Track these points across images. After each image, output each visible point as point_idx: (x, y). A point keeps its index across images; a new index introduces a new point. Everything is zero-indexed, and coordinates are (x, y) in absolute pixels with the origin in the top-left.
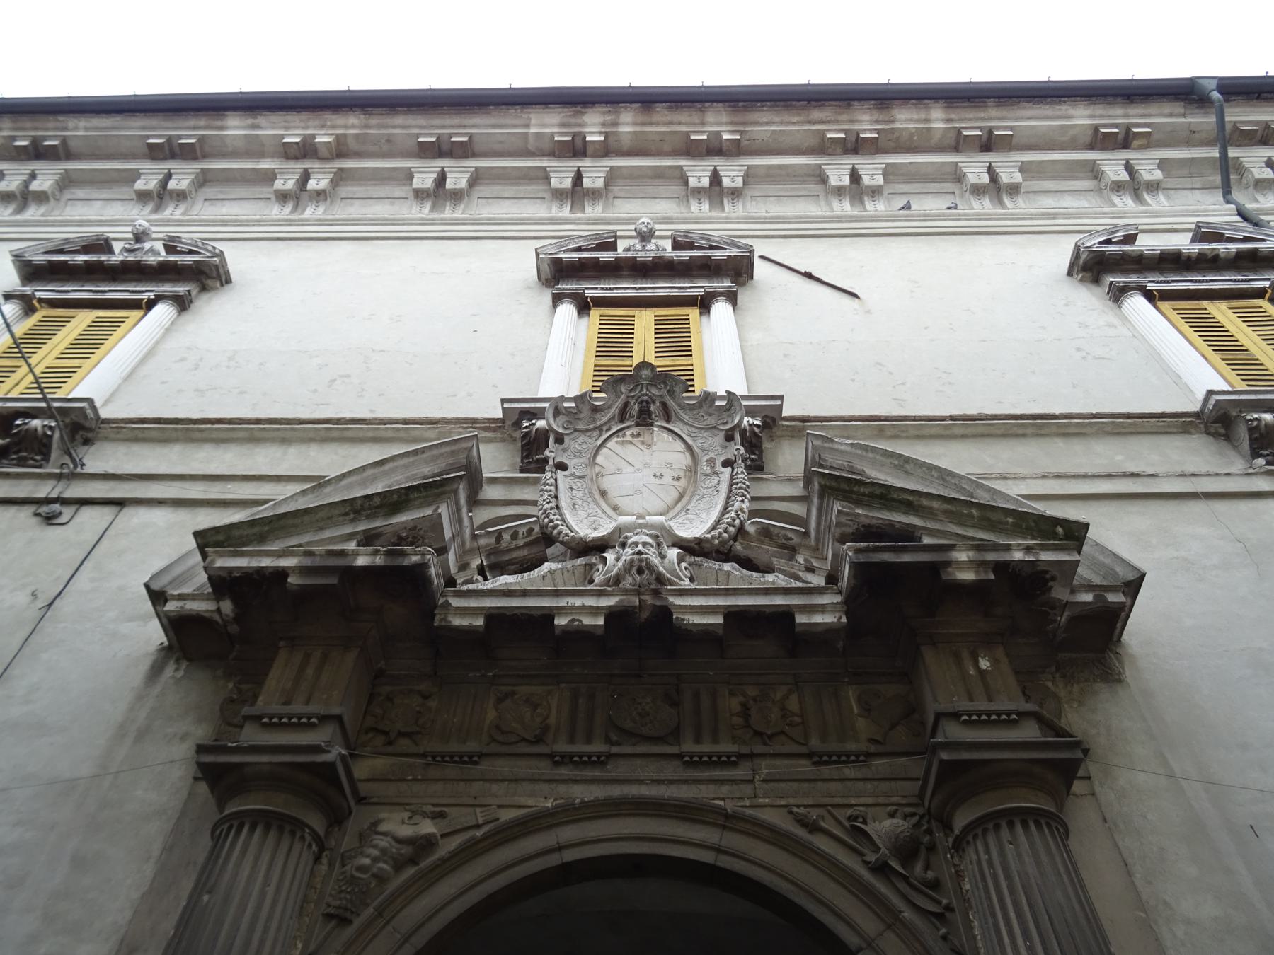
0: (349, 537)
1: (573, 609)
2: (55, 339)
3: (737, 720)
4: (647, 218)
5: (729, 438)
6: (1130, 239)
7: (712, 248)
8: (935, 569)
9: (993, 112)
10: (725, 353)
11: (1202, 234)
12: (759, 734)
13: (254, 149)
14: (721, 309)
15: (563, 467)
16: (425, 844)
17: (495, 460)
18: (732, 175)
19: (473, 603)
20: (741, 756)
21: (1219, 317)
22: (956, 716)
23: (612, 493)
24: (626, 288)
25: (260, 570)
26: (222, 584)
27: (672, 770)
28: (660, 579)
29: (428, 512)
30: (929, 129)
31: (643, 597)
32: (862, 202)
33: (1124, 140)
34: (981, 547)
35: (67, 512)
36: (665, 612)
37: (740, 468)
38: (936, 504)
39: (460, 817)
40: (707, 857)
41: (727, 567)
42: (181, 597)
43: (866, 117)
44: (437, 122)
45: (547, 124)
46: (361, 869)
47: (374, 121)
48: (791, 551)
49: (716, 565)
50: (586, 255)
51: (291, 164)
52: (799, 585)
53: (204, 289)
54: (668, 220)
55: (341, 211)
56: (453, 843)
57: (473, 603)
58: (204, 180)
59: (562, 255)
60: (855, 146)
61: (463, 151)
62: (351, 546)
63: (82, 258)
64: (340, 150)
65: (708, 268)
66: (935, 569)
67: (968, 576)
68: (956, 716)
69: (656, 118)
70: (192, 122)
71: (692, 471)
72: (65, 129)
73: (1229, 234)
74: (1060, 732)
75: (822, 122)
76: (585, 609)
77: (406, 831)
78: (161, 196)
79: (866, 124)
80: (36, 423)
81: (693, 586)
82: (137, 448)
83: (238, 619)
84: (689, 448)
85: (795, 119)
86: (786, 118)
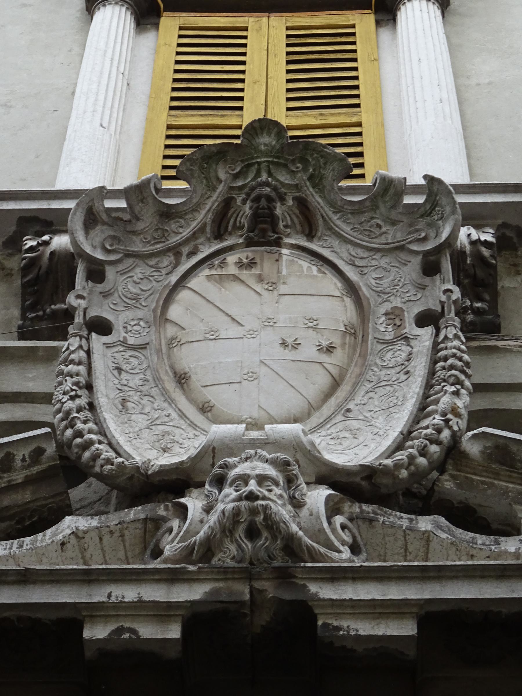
1: (120, 609)
5: (430, 268)
15: (102, 327)
23: (197, 380)
28: (291, 547)
31: (258, 585)
36: (302, 614)
37: (452, 330)
41: (425, 523)
49: (404, 520)
71: (357, 334)
81: (358, 562)
84: (352, 289)
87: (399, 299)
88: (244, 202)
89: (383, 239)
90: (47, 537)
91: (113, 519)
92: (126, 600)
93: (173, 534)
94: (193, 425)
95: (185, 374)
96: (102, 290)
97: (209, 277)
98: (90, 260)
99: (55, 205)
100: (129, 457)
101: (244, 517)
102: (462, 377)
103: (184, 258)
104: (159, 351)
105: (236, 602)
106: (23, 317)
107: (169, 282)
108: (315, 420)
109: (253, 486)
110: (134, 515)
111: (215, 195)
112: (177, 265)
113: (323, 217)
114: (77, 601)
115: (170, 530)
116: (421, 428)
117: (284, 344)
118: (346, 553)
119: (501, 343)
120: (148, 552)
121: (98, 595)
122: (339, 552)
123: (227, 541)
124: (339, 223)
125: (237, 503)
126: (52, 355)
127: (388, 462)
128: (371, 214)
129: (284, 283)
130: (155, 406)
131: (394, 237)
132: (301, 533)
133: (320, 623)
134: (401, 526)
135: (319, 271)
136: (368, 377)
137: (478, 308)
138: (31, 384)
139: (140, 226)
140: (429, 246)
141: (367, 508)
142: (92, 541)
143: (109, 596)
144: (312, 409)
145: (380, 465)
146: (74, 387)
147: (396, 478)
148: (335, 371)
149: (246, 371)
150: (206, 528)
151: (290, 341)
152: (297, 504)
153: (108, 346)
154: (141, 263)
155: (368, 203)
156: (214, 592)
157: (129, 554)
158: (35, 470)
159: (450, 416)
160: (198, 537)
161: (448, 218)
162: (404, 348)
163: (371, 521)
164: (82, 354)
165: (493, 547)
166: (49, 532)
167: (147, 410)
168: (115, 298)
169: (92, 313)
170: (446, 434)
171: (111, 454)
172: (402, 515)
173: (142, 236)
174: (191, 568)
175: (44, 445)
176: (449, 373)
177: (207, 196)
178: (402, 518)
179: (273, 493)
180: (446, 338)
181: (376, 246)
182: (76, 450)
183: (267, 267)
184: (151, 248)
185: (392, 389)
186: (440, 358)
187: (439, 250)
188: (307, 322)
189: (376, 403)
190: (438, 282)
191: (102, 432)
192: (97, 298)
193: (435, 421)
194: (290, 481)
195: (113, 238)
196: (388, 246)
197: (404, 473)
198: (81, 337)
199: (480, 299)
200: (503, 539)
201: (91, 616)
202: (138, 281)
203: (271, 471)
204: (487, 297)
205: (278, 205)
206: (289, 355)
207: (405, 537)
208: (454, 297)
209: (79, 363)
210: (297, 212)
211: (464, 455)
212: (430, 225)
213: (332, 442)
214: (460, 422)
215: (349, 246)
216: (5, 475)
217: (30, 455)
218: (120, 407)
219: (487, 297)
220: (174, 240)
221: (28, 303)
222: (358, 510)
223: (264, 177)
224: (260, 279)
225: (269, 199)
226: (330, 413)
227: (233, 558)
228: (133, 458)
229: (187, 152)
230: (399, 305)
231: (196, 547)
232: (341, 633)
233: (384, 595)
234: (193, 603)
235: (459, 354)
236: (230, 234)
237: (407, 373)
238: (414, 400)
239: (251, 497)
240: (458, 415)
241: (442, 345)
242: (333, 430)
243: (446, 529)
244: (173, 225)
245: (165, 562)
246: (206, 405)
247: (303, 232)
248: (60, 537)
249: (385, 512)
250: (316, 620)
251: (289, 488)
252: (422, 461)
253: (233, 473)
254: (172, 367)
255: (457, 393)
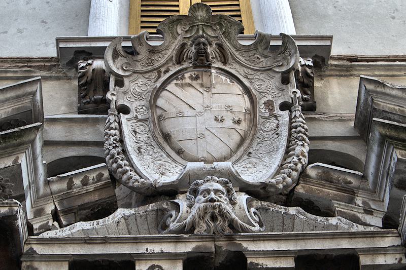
5: (285, 80)
15: (124, 110)
23: (175, 136)
28: (232, 224)
31: (218, 243)
41: (292, 211)
49: (282, 209)
84: (247, 91)
87: (270, 96)
88: (191, 45)
89: (261, 65)
90: (110, 219)
91: (141, 210)
92: (155, 252)
93: (173, 218)
94: (174, 160)
95: (168, 134)
96: (123, 91)
97: (176, 84)
98: (117, 75)
99: (94, 44)
100: (146, 178)
101: (210, 211)
102: (305, 137)
103: (162, 74)
104: (154, 122)
105: (208, 252)
106: (80, 102)
107: (156, 87)
108: (234, 158)
109: (213, 195)
110: (152, 207)
111: (176, 42)
112: (159, 77)
113: (230, 53)
114: (132, 253)
115: (171, 216)
116: (287, 163)
117: (216, 119)
118: (257, 227)
119: (317, 116)
120: (160, 226)
121: (142, 249)
122: (255, 226)
123: (201, 222)
124: (238, 56)
125: (205, 204)
126: (96, 121)
127: (273, 181)
128: (254, 52)
129: (214, 88)
130: (155, 150)
131: (266, 64)
132: (237, 218)
133: (249, 262)
134: (281, 212)
135: (231, 81)
136: (258, 136)
137: (305, 98)
138: (86, 137)
139: (140, 57)
140: (284, 69)
141: (264, 203)
142: (132, 221)
143: (147, 250)
144: (233, 152)
145: (270, 182)
146: (114, 142)
147: (277, 188)
148: (242, 133)
149: (199, 133)
150: (191, 215)
151: (219, 118)
152: (233, 202)
153: (129, 120)
154: (140, 76)
155: (252, 47)
156: (197, 247)
157: (150, 226)
158: (99, 184)
159: (301, 157)
160: (187, 220)
161: (293, 56)
162: (275, 121)
163: (267, 210)
164: (116, 124)
165: (325, 222)
166: (111, 216)
167: (151, 153)
168: (129, 95)
169: (120, 103)
170: (299, 166)
171: (138, 177)
172: (281, 207)
173: (141, 62)
174: (185, 236)
175: (103, 172)
176: (298, 135)
177: (172, 42)
178: (281, 208)
179: (222, 198)
180: (295, 116)
181: (258, 68)
182: (119, 175)
183: (205, 79)
184: (145, 69)
185: (270, 142)
186: (293, 127)
187: (288, 71)
188: (227, 108)
189: (263, 149)
190: (290, 88)
191: (131, 165)
192: (121, 95)
193: (294, 160)
194: (229, 191)
195: (127, 63)
196: (263, 69)
197: (281, 186)
198: (115, 115)
199: (306, 93)
200: (330, 218)
201: (139, 260)
202: (140, 86)
203: (220, 187)
204: (309, 93)
205: (209, 47)
206: (220, 125)
207: (283, 217)
208: (298, 96)
209: (115, 129)
210: (218, 50)
211: (308, 176)
212: (285, 58)
213: (243, 169)
214: (305, 159)
215: (244, 68)
216: (85, 187)
217: (96, 177)
218: (138, 152)
219: (309, 93)
220: (157, 65)
221: (82, 95)
222: (260, 204)
223: (201, 33)
224: (202, 85)
225: (204, 44)
226: (241, 154)
227: (205, 230)
228: (149, 179)
229: (161, 20)
230: (271, 99)
231: (187, 226)
232: (259, 266)
233: (278, 248)
234: (188, 253)
235: (302, 125)
236: (185, 61)
237: (277, 134)
238: (283, 149)
239: (212, 200)
240: (304, 156)
241: (294, 120)
242: (243, 163)
243: (303, 214)
244: (156, 57)
245: (171, 232)
246: (180, 151)
247: (221, 61)
248: (116, 219)
249: (273, 205)
250: (247, 261)
251: (229, 195)
252: (289, 180)
253: (202, 188)
254: (161, 131)
255: (303, 145)
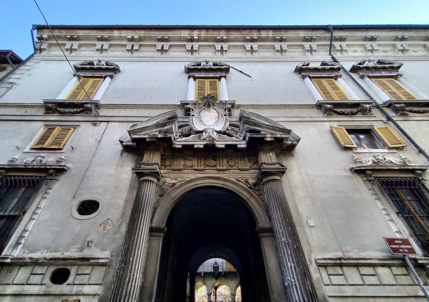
0: (157, 131)
1: (198, 144)
2: (87, 85)
3: (227, 163)
4: (207, 56)
5: (225, 110)
6: (308, 65)
7: (221, 66)
8: (263, 138)
9: (283, 33)
10: (225, 91)
11: (323, 64)
12: (230, 165)
13: (121, 38)
14: (223, 79)
15: (193, 116)
16: (174, 184)
17: (180, 113)
18: (225, 46)
19: (179, 143)
20: (227, 169)
21: (324, 83)
22: (265, 163)
23: (203, 121)
24: (203, 75)
25: (141, 138)
26: (133, 140)
27: (215, 171)
28: (213, 139)
29: (170, 126)
30: (268, 37)
32: (253, 53)
33: (311, 40)
34: (272, 134)
35: (98, 123)
36: (214, 145)
37: (227, 116)
38: (264, 126)
39: (179, 179)
40: (222, 186)
41: (225, 136)
42: (126, 142)
43: (255, 33)
44: (161, 33)
45: (185, 34)
46: (164, 188)
47: (147, 33)
48: (237, 133)
49: (223, 135)
50: (195, 67)
51: (130, 43)
52: (238, 140)
53: (115, 73)
54: (212, 58)
55: (141, 54)
56: (179, 184)
57: (179, 143)
58: (111, 46)
59: (190, 67)
60: (252, 40)
61: (167, 40)
62: (157, 133)
63: (88, 66)
64: (140, 39)
65: (221, 70)
66: (263, 138)
67: (269, 139)
68: (265, 163)
69: (209, 33)
70: (106, 32)
71: (218, 116)
72: (78, 33)
73: (329, 64)
74: (282, 166)
75: (245, 34)
76: (199, 144)
77: (171, 182)
78: (102, 50)
79: (255, 34)
80: (88, 105)
82: (109, 110)
83: (136, 146)
84: (218, 112)
85: (240, 34)
86: (238, 33)
